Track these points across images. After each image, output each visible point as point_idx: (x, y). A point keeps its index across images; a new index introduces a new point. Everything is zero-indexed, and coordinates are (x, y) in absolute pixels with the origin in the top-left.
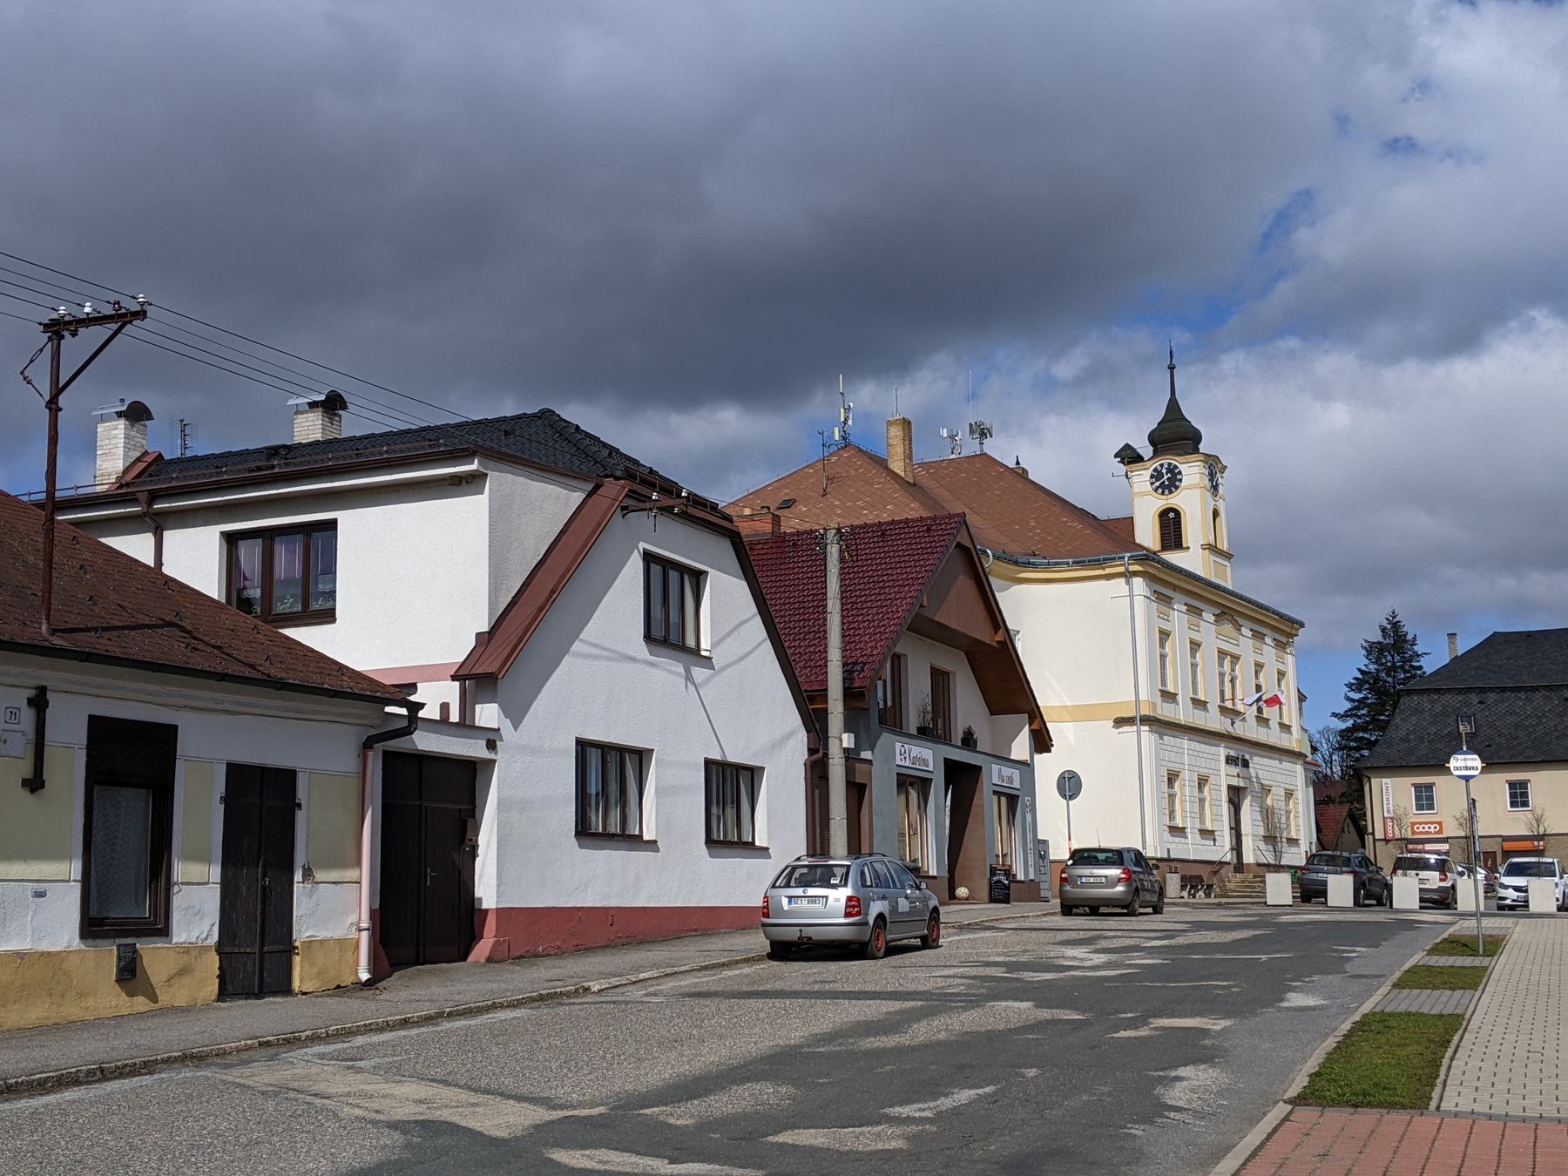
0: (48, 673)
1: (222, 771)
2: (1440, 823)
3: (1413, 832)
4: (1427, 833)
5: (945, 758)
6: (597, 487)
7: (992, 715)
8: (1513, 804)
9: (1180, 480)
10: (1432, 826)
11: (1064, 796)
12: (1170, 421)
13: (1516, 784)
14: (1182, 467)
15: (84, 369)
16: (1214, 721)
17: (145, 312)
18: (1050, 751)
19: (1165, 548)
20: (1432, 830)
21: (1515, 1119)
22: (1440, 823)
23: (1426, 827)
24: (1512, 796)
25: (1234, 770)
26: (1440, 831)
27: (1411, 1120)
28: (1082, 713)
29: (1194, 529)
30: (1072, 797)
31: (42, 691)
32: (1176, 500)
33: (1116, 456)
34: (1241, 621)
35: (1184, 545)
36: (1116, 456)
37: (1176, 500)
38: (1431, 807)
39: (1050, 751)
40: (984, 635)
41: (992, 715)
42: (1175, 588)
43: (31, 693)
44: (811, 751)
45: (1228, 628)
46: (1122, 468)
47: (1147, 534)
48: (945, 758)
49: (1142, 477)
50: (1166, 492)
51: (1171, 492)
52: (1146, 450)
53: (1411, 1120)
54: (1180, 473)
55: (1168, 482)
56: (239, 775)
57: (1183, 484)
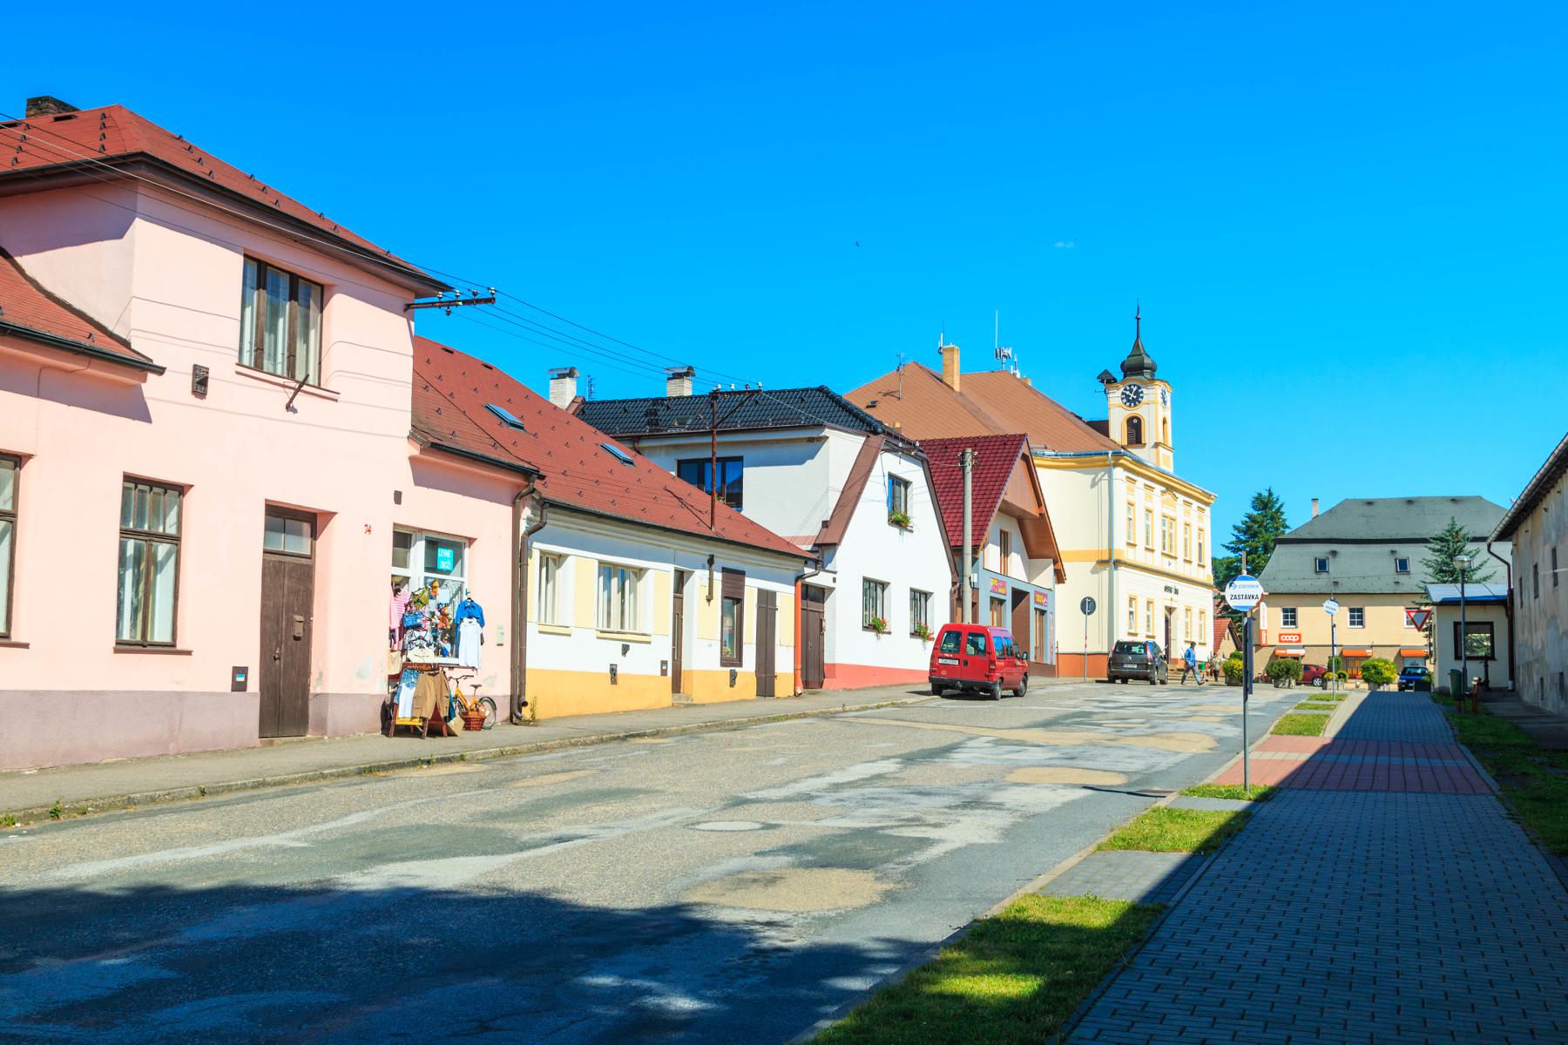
0: (714, 549)
1: (756, 591)
2: (1299, 635)
3: (1280, 641)
4: (1290, 642)
5: (1013, 588)
6: (868, 437)
7: (1030, 558)
8: (1352, 623)
9: (1142, 397)
10: (1294, 637)
11: (1085, 613)
12: (1134, 356)
13: (1295, 618)
14: (1145, 391)
15: (1339, 539)
16: (1157, 561)
17: (494, 299)
18: (1064, 583)
19: (1130, 443)
20: (1294, 640)
21: (1382, 791)
22: (1299, 635)
23: (1290, 637)
24: (1352, 617)
25: (1169, 595)
26: (1299, 641)
27: (1356, 743)
28: (1079, 556)
29: (1150, 434)
30: (1089, 614)
31: (712, 556)
32: (1140, 411)
33: (1098, 378)
34: (1177, 495)
35: (1143, 442)
36: (1098, 378)
37: (1140, 411)
38: (1294, 623)
39: (1064, 583)
40: (1032, 509)
41: (1030, 558)
42: (1138, 474)
43: (708, 558)
44: (954, 584)
45: (1168, 496)
46: (1102, 387)
47: (1118, 433)
48: (1013, 588)
49: (1116, 396)
50: (1133, 404)
51: (1135, 405)
52: (1119, 375)
53: (1356, 743)
54: (1142, 392)
55: (1133, 400)
56: (761, 592)
57: (1144, 401)
